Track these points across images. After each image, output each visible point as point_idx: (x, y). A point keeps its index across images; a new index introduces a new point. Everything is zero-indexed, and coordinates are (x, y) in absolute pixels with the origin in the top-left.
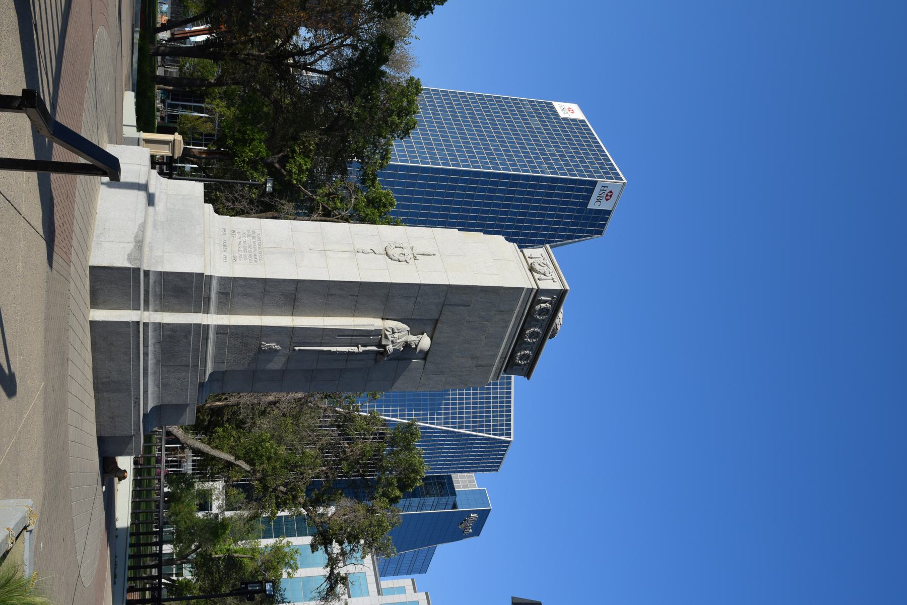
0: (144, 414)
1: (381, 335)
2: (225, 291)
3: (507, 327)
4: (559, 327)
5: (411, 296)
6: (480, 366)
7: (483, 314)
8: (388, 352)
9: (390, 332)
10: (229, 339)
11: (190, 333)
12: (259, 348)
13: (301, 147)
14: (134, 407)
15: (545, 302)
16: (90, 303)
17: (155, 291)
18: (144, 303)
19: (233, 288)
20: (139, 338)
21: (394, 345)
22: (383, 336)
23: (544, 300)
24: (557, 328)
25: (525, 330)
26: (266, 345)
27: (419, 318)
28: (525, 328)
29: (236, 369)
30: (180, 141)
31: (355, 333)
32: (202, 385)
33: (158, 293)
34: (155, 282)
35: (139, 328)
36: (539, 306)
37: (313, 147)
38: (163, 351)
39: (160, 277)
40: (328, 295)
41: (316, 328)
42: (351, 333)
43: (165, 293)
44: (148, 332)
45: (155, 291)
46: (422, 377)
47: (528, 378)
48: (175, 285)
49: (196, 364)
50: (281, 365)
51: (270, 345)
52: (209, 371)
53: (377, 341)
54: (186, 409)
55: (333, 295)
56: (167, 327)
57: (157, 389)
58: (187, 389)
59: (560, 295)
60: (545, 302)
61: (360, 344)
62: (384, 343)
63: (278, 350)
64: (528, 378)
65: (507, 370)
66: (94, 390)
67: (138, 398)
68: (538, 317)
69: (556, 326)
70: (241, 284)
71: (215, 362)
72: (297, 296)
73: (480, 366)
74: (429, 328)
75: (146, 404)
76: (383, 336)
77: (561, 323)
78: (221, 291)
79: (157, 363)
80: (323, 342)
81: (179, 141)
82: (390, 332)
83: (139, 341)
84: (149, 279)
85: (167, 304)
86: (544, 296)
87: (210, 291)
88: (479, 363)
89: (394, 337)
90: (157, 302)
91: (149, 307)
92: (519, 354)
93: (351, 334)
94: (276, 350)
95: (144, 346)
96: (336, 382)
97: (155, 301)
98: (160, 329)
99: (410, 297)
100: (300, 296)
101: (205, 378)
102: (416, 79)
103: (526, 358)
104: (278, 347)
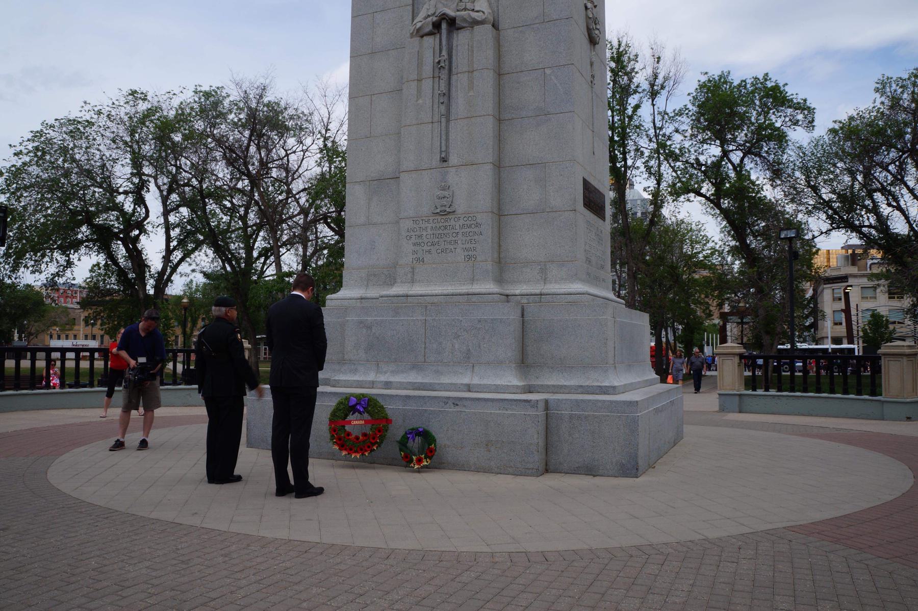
72: (373, 179)
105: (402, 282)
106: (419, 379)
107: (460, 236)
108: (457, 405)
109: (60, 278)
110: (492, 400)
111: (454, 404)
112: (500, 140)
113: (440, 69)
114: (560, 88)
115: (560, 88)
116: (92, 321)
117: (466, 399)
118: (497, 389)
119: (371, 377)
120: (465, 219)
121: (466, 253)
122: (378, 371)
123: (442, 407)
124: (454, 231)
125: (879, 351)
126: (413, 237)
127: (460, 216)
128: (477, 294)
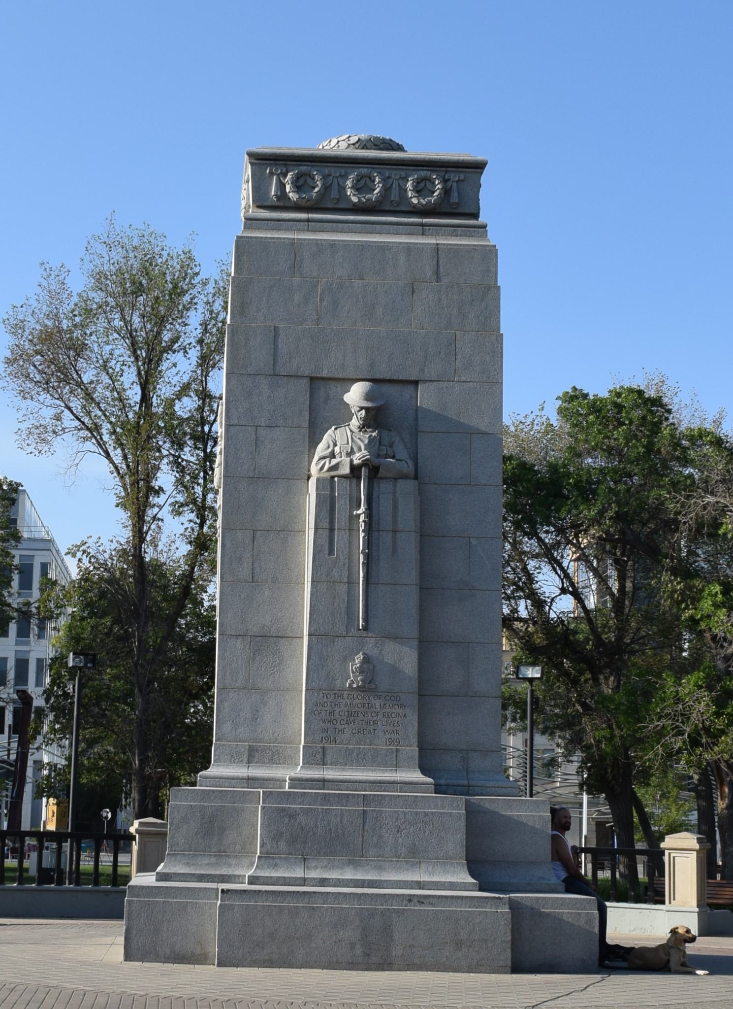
0: (480, 890)
1: (333, 477)
2: (246, 754)
3: (333, 245)
4: (354, 139)
5: (253, 436)
6: (437, 273)
7: (298, 298)
8: (367, 460)
9: (324, 464)
10: (341, 743)
11: (283, 810)
12: (362, 691)
13: (683, 606)
14: (432, 904)
15: (282, 186)
16: (201, 964)
17: (208, 864)
18: (228, 882)
19: (240, 741)
20: (446, 897)
21: (355, 449)
22: (333, 473)
23: (276, 190)
24: (357, 142)
25: (354, 204)
26: (352, 677)
27: (307, 414)
28: (350, 206)
29: (416, 728)
30: (140, 822)
31: (326, 524)
32: (438, 789)
33: (213, 860)
34: (188, 865)
35: (236, 891)
36: (291, 195)
37: (679, 583)
38: (325, 855)
39: (179, 857)
40: (253, 582)
41: (311, 595)
42: (325, 534)
43: (214, 850)
44: (271, 877)
45: (208, 864)
46: (463, 378)
47: (480, 166)
48: (197, 834)
49: (361, 799)
50: (406, 649)
51: (353, 672)
52: (417, 776)
53: (346, 483)
54: (503, 815)
55: (253, 573)
56: (268, 847)
57: (423, 866)
58: (426, 814)
59: (264, 162)
60: (282, 186)
61: (351, 512)
62: (346, 470)
63: (364, 658)
64: (480, 166)
65: (471, 210)
66: (383, 970)
67: (410, 899)
68: (316, 190)
69: (353, 144)
70: (230, 728)
71: (397, 766)
72: (257, 634)
73: (437, 273)
74: (334, 388)
75: (464, 887)
76: (333, 473)
77: (348, 136)
78: (246, 760)
79: (354, 863)
80: (346, 580)
81: (139, 826)
82: (324, 464)
83: (266, 891)
84: (175, 874)
85: (238, 847)
86: (269, 191)
87: (233, 779)
88: (429, 273)
89: (340, 452)
90: (233, 861)
91: (235, 876)
92: (415, 201)
93: (327, 532)
94: (367, 660)
95: (304, 885)
96: (474, 542)
97: (230, 865)
98: (274, 858)
99: (257, 439)
100: (255, 629)
101: (427, 784)
102: (560, 402)
103: (428, 183)
104: (359, 659)
105: (331, 764)
106: (360, 876)
107: (380, 716)
108: (423, 903)
109: (554, 425)
110: (462, 898)
111: (419, 902)
112: (422, 610)
113: (178, 562)
114: (487, 562)
115: (487, 562)
116: (124, 781)
117: (429, 896)
118: (452, 886)
119: (299, 873)
120: (387, 698)
121: (387, 736)
122: (306, 868)
123: (406, 906)
124: (374, 710)
125: (662, 845)
126: (323, 713)
127: (380, 694)
128: (409, 784)
